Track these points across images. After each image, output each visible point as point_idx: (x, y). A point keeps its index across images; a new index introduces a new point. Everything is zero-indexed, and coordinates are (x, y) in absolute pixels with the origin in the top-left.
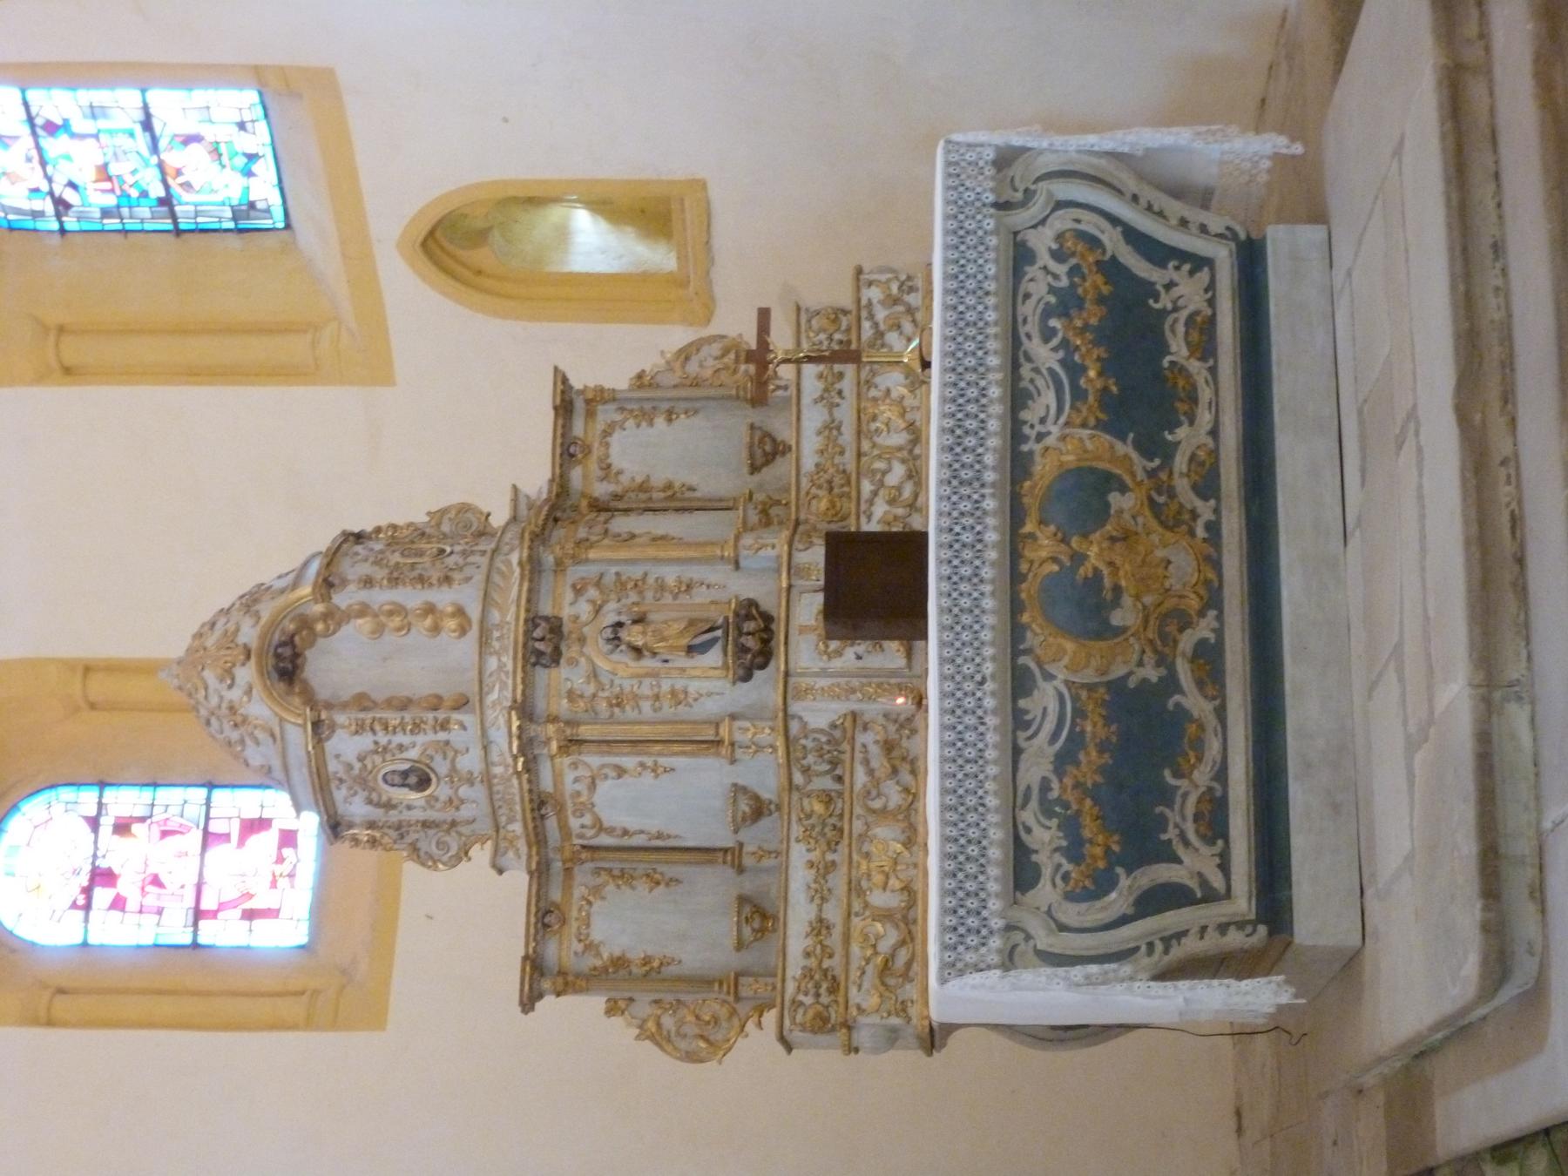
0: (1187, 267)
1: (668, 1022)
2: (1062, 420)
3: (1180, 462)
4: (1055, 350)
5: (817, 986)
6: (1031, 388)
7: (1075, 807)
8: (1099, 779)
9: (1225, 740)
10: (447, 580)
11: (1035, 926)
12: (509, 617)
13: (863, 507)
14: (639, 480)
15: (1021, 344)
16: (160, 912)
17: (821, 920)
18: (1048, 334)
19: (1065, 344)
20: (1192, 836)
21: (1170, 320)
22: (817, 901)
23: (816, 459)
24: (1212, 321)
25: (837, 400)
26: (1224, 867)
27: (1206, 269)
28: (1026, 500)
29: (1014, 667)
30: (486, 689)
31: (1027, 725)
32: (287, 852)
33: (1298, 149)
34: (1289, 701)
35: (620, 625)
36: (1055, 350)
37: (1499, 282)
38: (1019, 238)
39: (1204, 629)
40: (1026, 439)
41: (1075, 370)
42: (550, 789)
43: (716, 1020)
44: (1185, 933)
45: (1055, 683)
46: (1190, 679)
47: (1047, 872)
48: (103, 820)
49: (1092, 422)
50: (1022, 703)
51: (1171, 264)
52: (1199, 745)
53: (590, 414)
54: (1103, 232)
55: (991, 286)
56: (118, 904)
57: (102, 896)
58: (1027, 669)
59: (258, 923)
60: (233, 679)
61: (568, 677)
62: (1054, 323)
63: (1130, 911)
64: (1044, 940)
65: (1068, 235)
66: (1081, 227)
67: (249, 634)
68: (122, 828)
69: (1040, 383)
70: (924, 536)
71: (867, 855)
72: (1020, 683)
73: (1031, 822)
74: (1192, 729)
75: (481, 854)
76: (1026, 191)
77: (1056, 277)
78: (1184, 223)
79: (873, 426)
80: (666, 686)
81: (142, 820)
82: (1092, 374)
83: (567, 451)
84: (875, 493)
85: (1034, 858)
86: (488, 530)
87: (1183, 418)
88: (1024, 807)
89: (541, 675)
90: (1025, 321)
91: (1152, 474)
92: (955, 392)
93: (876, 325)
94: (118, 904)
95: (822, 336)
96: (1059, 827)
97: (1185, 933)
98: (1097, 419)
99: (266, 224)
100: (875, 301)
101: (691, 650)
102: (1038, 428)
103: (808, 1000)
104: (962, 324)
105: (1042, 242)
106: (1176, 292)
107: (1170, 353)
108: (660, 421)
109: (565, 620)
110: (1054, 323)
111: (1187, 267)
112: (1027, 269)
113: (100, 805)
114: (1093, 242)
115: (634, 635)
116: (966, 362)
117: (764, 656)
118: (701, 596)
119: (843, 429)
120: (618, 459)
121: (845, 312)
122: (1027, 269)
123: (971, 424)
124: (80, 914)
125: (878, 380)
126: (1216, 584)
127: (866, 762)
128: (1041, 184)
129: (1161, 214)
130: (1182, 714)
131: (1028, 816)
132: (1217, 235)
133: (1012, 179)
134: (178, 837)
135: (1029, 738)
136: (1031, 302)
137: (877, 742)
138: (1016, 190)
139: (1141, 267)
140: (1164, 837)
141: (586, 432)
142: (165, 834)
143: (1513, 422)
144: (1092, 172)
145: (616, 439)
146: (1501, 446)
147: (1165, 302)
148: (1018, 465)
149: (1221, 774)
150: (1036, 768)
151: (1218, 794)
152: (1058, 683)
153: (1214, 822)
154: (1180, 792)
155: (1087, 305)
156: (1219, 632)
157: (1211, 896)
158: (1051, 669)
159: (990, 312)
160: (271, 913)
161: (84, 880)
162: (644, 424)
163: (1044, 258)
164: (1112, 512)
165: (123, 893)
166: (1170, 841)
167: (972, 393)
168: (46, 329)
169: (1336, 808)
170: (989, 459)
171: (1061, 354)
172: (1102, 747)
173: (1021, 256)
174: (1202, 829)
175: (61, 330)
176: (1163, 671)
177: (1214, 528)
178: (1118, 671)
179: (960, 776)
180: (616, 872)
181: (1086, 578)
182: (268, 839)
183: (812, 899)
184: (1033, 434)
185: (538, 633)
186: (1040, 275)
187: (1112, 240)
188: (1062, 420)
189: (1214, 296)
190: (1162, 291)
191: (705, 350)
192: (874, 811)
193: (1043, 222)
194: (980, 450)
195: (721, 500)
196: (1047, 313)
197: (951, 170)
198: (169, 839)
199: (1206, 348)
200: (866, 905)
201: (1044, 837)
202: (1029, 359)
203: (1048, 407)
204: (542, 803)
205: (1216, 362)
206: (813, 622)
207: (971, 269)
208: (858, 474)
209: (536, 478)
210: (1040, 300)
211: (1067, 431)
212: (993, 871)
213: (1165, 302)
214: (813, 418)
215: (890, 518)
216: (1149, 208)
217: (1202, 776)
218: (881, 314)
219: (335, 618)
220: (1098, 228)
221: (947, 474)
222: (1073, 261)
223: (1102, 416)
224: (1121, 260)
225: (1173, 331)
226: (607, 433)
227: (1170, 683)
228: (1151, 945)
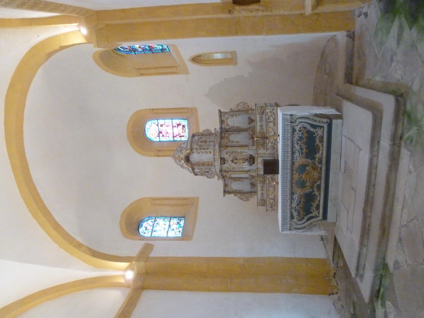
0: (320, 128)
1: (242, 197)
2: (300, 157)
3: (317, 159)
4: (299, 146)
5: (262, 201)
6: (295, 152)
7: (299, 210)
8: (303, 206)
9: (320, 198)
10: (208, 149)
11: (294, 224)
12: (217, 157)
13: (267, 144)
14: (232, 126)
15: (293, 145)
16: (169, 137)
17: (262, 193)
18: (298, 144)
19: (300, 146)
20: (315, 210)
21: (317, 137)
22: (262, 191)
23: (259, 130)
24: (323, 137)
25: (262, 121)
26: (319, 213)
27: (323, 128)
28: (294, 169)
29: (292, 191)
30: (215, 166)
31: (293, 199)
32: (184, 128)
33: (340, 114)
34: (329, 192)
35: (232, 160)
36: (299, 146)
37: (373, 190)
38: (294, 127)
39: (318, 183)
40: (294, 159)
41: (302, 149)
42: (227, 183)
43: (248, 197)
44: (313, 222)
45: (297, 195)
46: (316, 190)
47: (295, 218)
48: (159, 125)
49: (304, 157)
50: (293, 196)
51: (317, 128)
52: (316, 199)
53: (224, 115)
54: (307, 126)
55: (289, 138)
56: (163, 136)
57: (161, 135)
58: (293, 192)
59: (181, 138)
60: (181, 162)
61: (225, 167)
62: (299, 142)
63: (306, 221)
64: (295, 226)
65: (301, 127)
66: (304, 126)
67: (182, 156)
68: (161, 126)
69: (296, 151)
70: (278, 160)
71: (269, 191)
72: (292, 194)
73: (293, 211)
74: (316, 196)
75: (216, 177)
76: (295, 120)
77: (299, 134)
78: (320, 122)
79: (268, 132)
80: (240, 166)
81: (164, 124)
82: (304, 150)
83: (222, 122)
84: (269, 142)
85: (294, 216)
86: (211, 133)
87: (317, 153)
88: (292, 209)
89: (223, 165)
90: (294, 141)
91: (312, 163)
92: (283, 157)
93: (269, 116)
94: (163, 136)
95: (259, 111)
96: (297, 213)
97: (313, 222)
98: (305, 157)
99: (166, 51)
100: (268, 112)
101: (243, 163)
102: (296, 158)
103: (261, 202)
104: (285, 144)
105: (297, 128)
106: (318, 132)
107: (316, 143)
108: (235, 117)
109: (225, 158)
110: (299, 142)
111: (320, 128)
112: (295, 132)
113: (158, 123)
114: (305, 128)
115: (235, 161)
116: (285, 150)
117: (254, 163)
118: (244, 154)
119: (263, 126)
120: (229, 123)
121: (263, 107)
122: (295, 132)
123: (286, 160)
124: (158, 137)
125: (269, 125)
126: (321, 176)
127: (269, 180)
128: (297, 120)
129: (316, 121)
130: (315, 195)
131: (293, 210)
132: (325, 123)
133: (293, 118)
134: (169, 127)
135: (294, 201)
136: (295, 138)
137: (270, 177)
138: (293, 120)
139: (312, 130)
140: (311, 211)
141: (224, 119)
142: (167, 126)
143: (371, 211)
144: (306, 117)
145: (229, 120)
146: (369, 214)
147: (316, 135)
148: (293, 163)
149: (319, 202)
150: (294, 205)
151: (319, 204)
152: (298, 195)
153: (318, 207)
154: (313, 205)
155: (304, 139)
156: (320, 183)
157: (316, 217)
158: (297, 193)
159: (289, 135)
160: (183, 136)
161: (158, 133)
162: (232, 117)
163: (298, 131)
164: (306, 170)
165: (163, 134)
166: (312, 211)
167: (286, 155)
168: (137, 69)
169: (334, 206)
170: (289, 165)
171: (300, 147)
172: (304, 202)
173: (294, 130)
174: (316, 209)
175: (139, 69)
176: (312, 190)
177: (321, 168)
178: (306, 192)
179: (284, 208)
180: (234, 180)
181: (302, 180)
182: (181, 126)
183: (261, 191)
184: (295, 159)
185: (222, 161)
186: (297, 134)
187: (308, 127)
188: (300, 157)
189: (324, 132)
190: (315, 133)
191: (241, 105)
192: (270, 186)
193: (297, 125)
194: (287, 164)
195: (245, 129)
196: (298, 140)
197: (283, 119)
198: (168, 127)
199: (322, 141)
200: (269, 197)
201: (295, 214)
202: (295, 147)
203: (297, 155)
204: (224, 177)
205: (323, 143)
206: (261, 162)
207: (286, 135)
208: (266, 133)
209: (218, 127)
210: (297, 138)
211: (301, 159)
212: (288, 209)
213: (316, 135)
214: (258, 124)
215: (271, 146)
216: (315, 120)
217: (317, 202)
218: (269, 114)
219: (193, 153)
220: (306, 125)
221: (283, 162)
222: (302, 132)
223: (305, 156)
224: (310, 130)
225: (317, 139)
226: (227, 119)
227: (314, 191)
228: (308, 225)
